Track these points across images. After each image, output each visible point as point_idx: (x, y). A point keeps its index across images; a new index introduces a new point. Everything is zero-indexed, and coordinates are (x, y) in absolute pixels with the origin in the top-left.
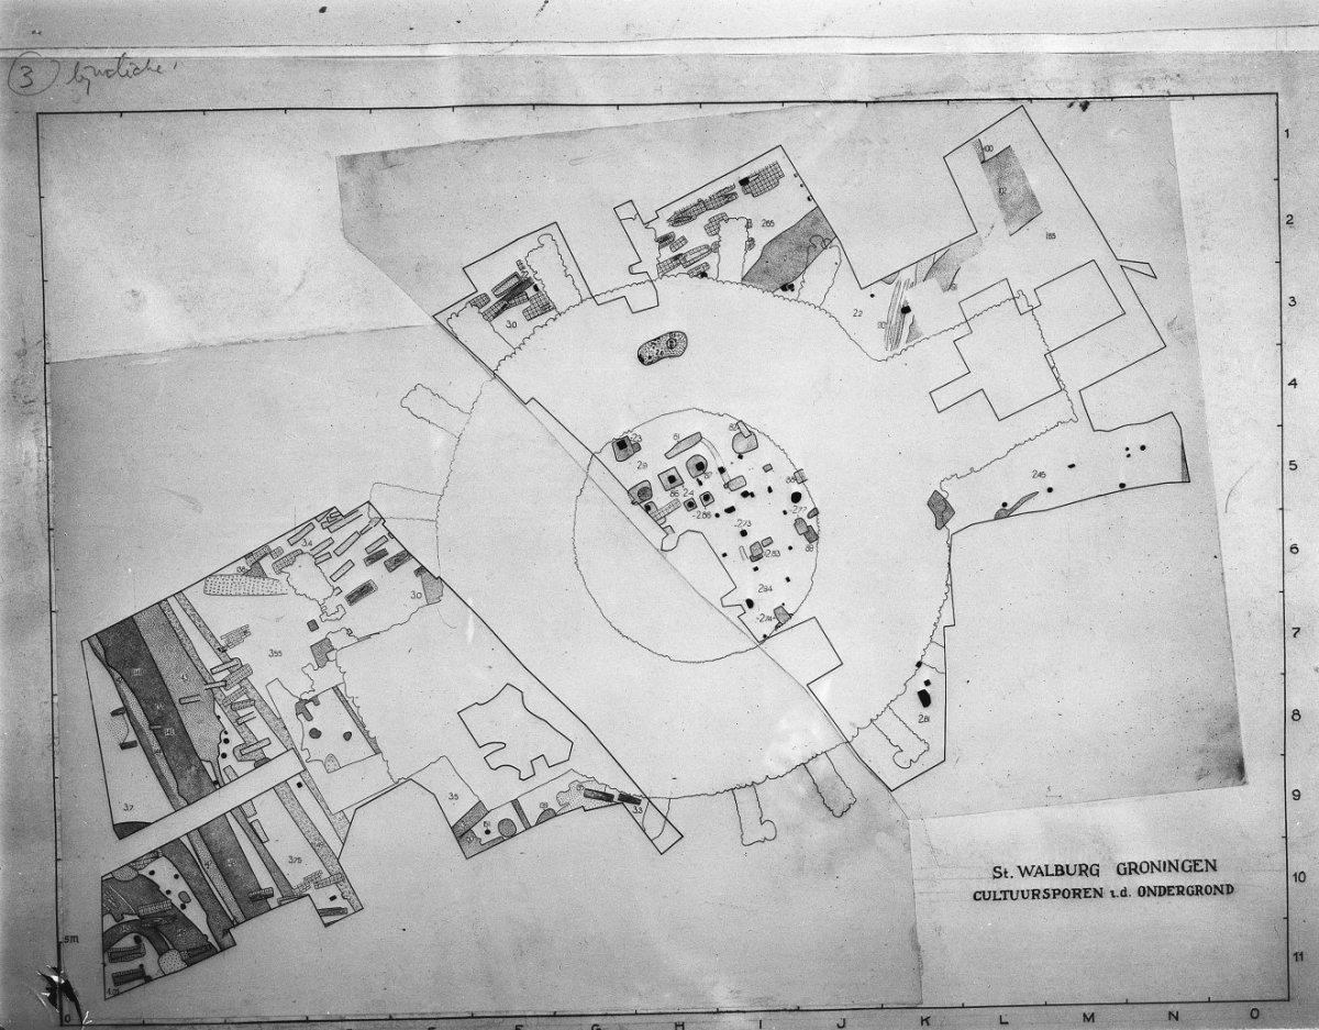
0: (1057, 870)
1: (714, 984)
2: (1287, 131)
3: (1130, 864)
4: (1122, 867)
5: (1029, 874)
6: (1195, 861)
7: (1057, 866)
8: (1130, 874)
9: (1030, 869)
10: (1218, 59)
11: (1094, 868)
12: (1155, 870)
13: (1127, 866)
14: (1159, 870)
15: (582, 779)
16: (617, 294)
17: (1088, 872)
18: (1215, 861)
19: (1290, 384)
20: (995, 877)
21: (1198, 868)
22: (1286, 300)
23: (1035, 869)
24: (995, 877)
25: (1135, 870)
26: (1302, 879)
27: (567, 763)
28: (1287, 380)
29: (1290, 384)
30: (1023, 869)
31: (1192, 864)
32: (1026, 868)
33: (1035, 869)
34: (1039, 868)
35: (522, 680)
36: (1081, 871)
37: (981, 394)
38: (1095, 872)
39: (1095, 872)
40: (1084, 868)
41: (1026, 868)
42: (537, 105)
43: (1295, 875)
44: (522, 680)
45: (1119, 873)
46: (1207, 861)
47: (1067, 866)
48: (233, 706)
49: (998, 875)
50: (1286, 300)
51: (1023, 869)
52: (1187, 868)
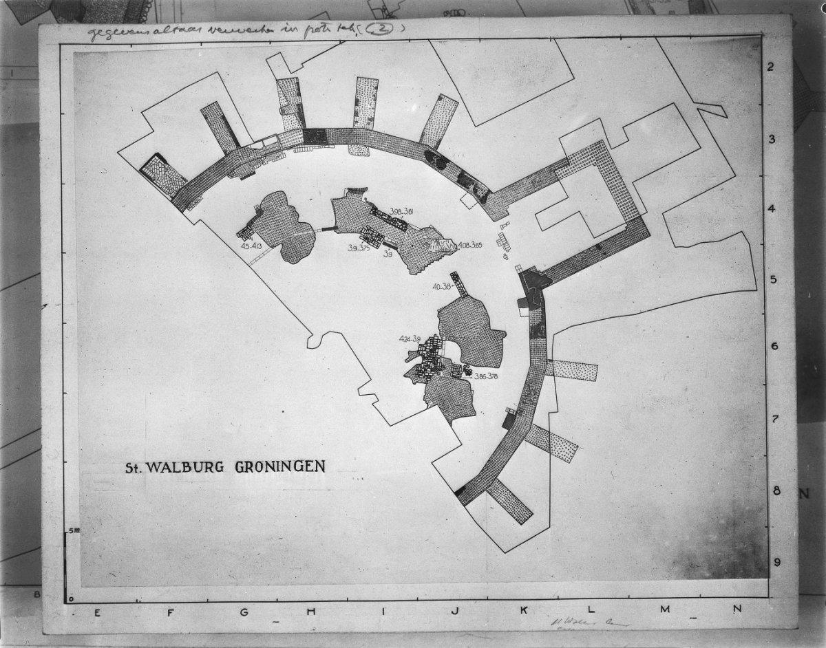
0: (184, 467)
1: (37, 615)
3: (247, 462)
4: (240, 465)
6: (307, 462)
7: (184, 463)
8: (247, 471)
9: (157, 465)
11: (219, 465)
12: (269, 469)
14: (273, 469)
17: (213, 469)
18: (323, 461)
19: (769, 209)
20: (127, 472)
21: (309, 468)
24: (127, 472)
25: (210, 468)
27: (332, 329)
28: (767, 206)
29: (769, 209)
30: (151, 465)
31: (304, 464)
32: (154, 464)
34: (166, 464)
36: (207, 468)
38: (219, 469)
39: (219, 469)
40: (249, 465)
41: (154, 464)
42: (762, 107)
45: (237, 470)
46: (317, 462)
47: (195, 463)
48: (785, 272)
52: (298, 467)
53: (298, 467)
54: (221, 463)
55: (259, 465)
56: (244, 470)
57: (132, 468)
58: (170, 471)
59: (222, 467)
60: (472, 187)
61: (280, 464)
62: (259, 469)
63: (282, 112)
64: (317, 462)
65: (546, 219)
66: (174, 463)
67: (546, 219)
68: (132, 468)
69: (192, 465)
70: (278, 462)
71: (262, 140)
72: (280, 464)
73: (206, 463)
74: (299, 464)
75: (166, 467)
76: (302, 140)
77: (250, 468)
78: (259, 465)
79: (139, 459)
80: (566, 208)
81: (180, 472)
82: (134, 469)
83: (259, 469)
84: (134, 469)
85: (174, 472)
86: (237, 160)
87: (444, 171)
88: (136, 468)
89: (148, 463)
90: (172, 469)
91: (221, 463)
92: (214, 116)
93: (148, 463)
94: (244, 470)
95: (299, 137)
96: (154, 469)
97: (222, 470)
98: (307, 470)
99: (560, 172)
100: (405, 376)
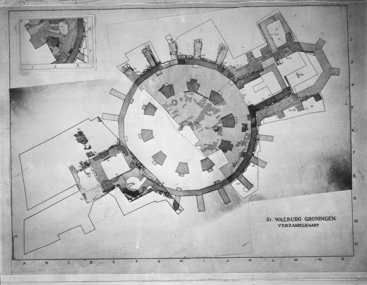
2: (350, 16)
4: (306, 218)
5: (278, 220)
6: (329, 217)
7: (287, 218)
8: (309, 220)
9: (278, 219)
10: (324, 3)
11: (300, 218)
12: (323, 218)
13: (308, 218)
14: (322, 218)
15: (226, 46)
16: (87, 47)
17: (298, 220)
20: (267, 221)
21: (330, 219)
22: (350, 62)
23: (280, 219)
26: (357, 222)
30: (276, 219)
32: (277, 219)
33: (280, 219)
34: (281, 219)
35: (145, 44)
36: (295, 220)
37: (94, 229)
38: (300, 220)
39: (300, 220)
41: (277, 219)
43: (355, 220)
44: (145, 44)
46: (332, 217)
47: (291, 218)
49: (268, 220)
50: (350, 62)
51: (276, 219)
52: (326, 219)
53: (326, 219)
54: (300, 218)
55: (313, 218)
56: (308, 220)
57: (268, 220)
58: (282, 221)
59: (301, 219)
60: (232, 78)
61: (321, 218)
62: (313, 220)
63: (171, 54)
64: (332, 217)
65: (256, 88)
66: (284, 218)
67: (256, 88)
68: (268, 220)
69: (290, 219)
70: (320, 217)
71: (164, 63)
72: (321, 218)
73: (295, 218)
74: (326, 218)
75: (281, 220)
76: (177, 63)
77: (310, 220)
78: (313, 218)
79: (271, 216)
80: (263, 85)
81: (286, 221)
82: (270, 220)
83: (313, 220)
84: (270, 220)
85: (284, 221)
86: (155, 68)
87: (223, 73)
88: (271, 219)
89: (275, 218)
90: (283, 220)
91: (300, 218)
92: (148, 52)
93: (275, 218)
94: (308, 220)
95: (176, 62)
96: (277, 220)
97: (301, 220)
98: (329, 220)
99: (261, 73)
100: (140, 181)
